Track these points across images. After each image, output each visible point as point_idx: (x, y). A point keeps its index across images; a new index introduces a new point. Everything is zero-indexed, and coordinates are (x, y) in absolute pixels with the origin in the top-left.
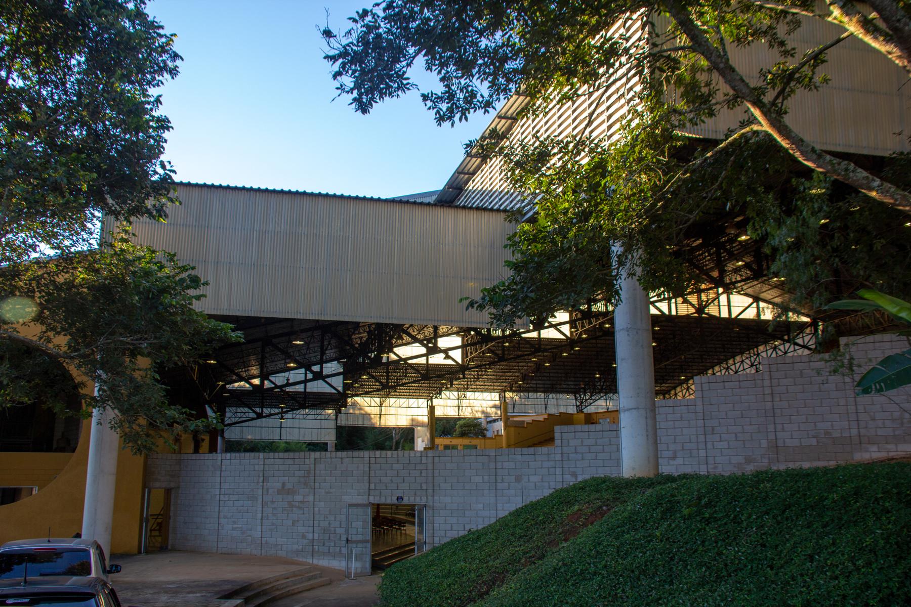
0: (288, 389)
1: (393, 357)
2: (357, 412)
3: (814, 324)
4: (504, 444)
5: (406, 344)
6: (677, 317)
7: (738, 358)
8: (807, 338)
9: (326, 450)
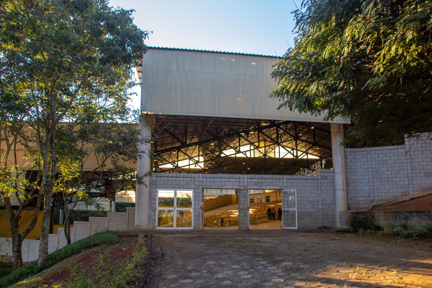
2: (127, 197)
3: (321, 160)
6: (254, 158)
7: (313, 165)
8: (317, 166)
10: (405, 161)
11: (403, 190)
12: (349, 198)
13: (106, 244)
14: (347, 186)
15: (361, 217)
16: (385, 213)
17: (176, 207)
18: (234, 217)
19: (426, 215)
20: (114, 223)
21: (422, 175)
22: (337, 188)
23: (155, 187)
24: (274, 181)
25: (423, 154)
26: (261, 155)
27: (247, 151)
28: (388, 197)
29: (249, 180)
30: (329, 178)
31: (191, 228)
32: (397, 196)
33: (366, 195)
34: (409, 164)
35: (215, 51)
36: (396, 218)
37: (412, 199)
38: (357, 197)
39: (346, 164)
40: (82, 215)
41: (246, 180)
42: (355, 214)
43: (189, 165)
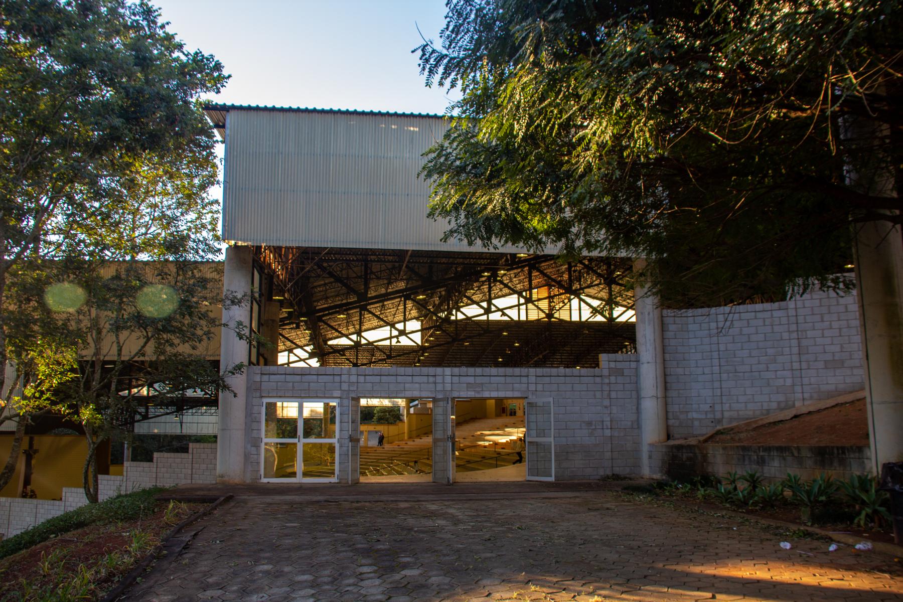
0: (291, 365)
1: (460, 316)
4: (406, 438)
5: (503, 296)
6: (528, 322)
9: (187, 452)
10: (786, 335)
11: (781, 398)
12: (670, 416)
13: (102, 523)
14: (666, 389)
15: (685, 456)
16: (725, 448)
17: (302, 436)
18: (485, 447)
19: (793, 455)
20: (204, 466)
21: (821, 365)
22: (643, 393)
23: (258, 395)
24: (509, 379)
25: (822, 321)
26: (542, 315)
27: (509, 307)
28: (751, 413)
29: (456, 379)
30: (626, 372)
31: (334, 480)
32: (768, 411)
33: (706, 407)
34: (794, 343)
35: (376, 110)
36: (744, 460)
37: (796, 416)
38: (687, 412)
39: (663, 342)
40: (174, 443)
41: (448, 379)
42: (674, 450)
43: (391, 338)
